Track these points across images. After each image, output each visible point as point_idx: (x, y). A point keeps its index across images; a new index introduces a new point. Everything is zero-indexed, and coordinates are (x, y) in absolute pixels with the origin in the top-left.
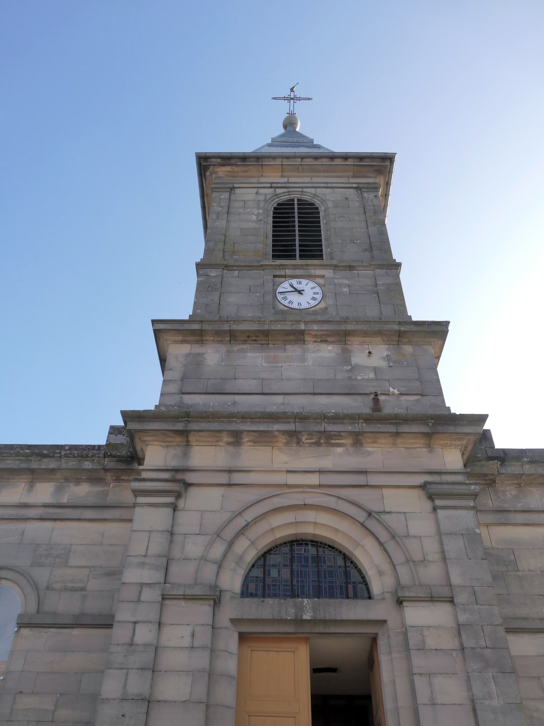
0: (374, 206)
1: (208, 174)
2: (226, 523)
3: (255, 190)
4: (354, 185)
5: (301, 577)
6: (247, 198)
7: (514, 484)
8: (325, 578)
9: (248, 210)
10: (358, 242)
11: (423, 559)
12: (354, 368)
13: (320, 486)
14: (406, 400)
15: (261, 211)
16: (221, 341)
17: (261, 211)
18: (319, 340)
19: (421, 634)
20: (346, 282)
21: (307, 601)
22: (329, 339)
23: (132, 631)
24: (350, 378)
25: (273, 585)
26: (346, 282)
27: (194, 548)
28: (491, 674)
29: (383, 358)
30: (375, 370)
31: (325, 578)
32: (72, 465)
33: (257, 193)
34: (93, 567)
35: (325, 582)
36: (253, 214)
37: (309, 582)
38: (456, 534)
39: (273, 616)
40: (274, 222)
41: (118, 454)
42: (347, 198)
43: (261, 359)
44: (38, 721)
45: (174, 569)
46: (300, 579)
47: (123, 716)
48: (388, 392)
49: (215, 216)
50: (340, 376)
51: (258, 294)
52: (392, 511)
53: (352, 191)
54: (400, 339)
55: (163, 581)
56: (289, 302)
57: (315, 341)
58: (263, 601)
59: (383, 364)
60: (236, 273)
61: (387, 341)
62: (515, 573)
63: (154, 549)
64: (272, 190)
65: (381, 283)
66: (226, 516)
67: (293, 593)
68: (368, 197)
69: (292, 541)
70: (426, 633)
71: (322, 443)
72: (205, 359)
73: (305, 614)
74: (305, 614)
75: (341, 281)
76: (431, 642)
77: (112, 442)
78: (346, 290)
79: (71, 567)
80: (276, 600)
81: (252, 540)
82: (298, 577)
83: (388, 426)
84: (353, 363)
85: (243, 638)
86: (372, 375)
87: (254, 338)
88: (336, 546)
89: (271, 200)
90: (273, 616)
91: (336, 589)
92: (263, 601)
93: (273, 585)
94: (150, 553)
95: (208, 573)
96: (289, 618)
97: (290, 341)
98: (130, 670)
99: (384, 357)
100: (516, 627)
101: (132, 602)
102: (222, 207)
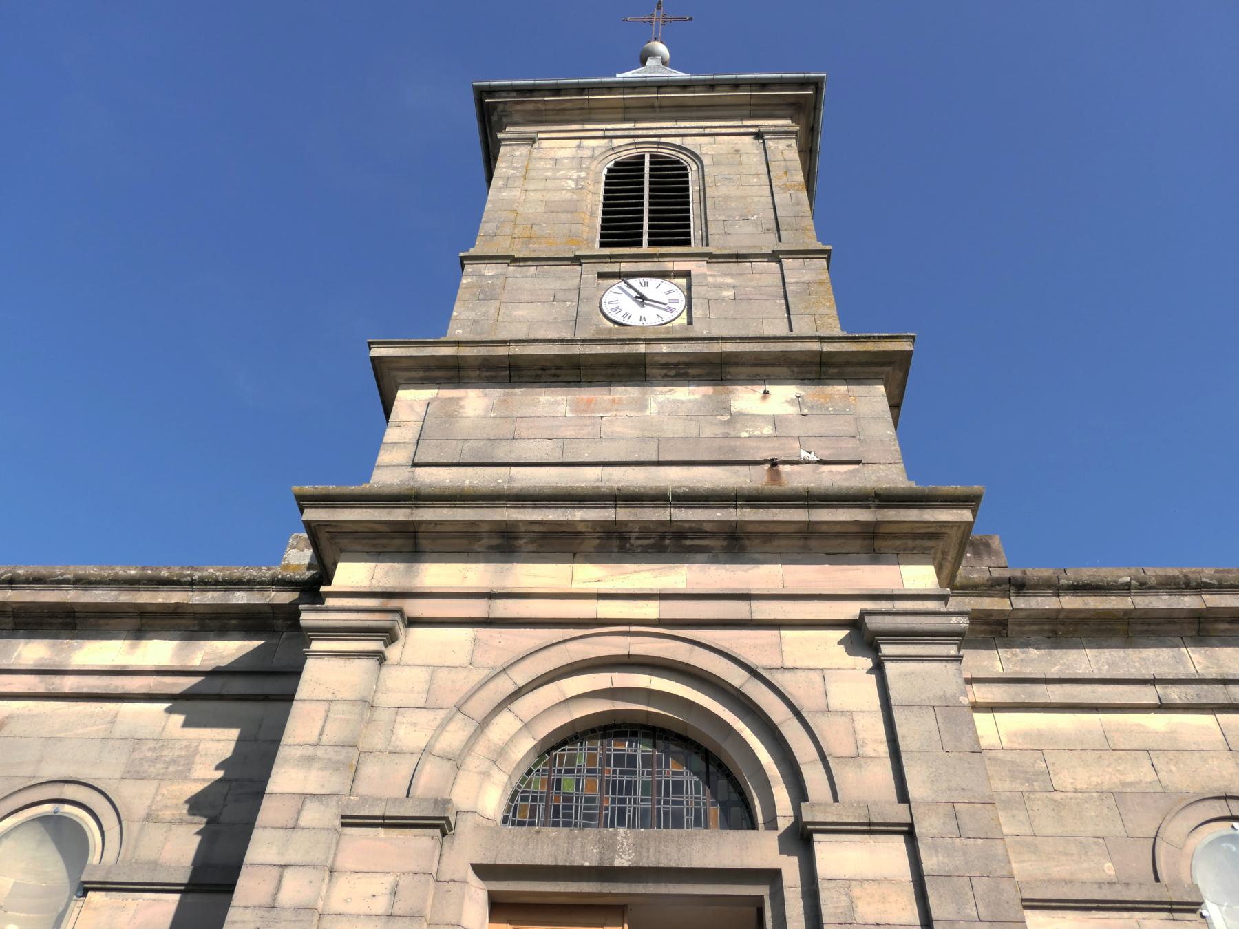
4: (751, 130)
5: (621, 793)
6: (561, 153)
7: (1042, 631)
8: (667, 794)
11: (854, 753)
12: (736, 418)
13: (660, 623)
15: (583, 174)
16: (493, 377)
17: (583, 174)
18: (673, 372)
20: (729, 281)
22: (692, 371)
23: (275, 883)
24: (726, 436)
25: (564, 808)
26: (729, 281)
27: (412, 733)
29: (791, 402)
30: (775, 420)
31: (667, 794)
33: (579, 146)
34: (236, 780)
35: (666, 802)
38: (920, 707)
42: (737, 151)
45: (370, 770)
50: (708, 432)
52: (798, 665)
53: (748, 139)
55: (347, 790)
56: (624, 316)
57: (666, 376)
58: (538, 832)
62: (1048, 794)
63: (334, 732)
66: (477, 676)
70: (856, 891)
71: (667, 547)
72: (462, 407)
75: (720, 280)
77: (292, 562)
78: (729, 294)
79: (195, 780)
81: (526, 721)
82: (613, 793)
84: (733, 409)
86: (768, 430)
87: (553, 371)
88: (691, 736)
92: (538, 832)
93: (564, 808)
94: (325, 739)
95: (430, 778)
96: (587, 864)
97: (620, 375)
100: (1049, 896)
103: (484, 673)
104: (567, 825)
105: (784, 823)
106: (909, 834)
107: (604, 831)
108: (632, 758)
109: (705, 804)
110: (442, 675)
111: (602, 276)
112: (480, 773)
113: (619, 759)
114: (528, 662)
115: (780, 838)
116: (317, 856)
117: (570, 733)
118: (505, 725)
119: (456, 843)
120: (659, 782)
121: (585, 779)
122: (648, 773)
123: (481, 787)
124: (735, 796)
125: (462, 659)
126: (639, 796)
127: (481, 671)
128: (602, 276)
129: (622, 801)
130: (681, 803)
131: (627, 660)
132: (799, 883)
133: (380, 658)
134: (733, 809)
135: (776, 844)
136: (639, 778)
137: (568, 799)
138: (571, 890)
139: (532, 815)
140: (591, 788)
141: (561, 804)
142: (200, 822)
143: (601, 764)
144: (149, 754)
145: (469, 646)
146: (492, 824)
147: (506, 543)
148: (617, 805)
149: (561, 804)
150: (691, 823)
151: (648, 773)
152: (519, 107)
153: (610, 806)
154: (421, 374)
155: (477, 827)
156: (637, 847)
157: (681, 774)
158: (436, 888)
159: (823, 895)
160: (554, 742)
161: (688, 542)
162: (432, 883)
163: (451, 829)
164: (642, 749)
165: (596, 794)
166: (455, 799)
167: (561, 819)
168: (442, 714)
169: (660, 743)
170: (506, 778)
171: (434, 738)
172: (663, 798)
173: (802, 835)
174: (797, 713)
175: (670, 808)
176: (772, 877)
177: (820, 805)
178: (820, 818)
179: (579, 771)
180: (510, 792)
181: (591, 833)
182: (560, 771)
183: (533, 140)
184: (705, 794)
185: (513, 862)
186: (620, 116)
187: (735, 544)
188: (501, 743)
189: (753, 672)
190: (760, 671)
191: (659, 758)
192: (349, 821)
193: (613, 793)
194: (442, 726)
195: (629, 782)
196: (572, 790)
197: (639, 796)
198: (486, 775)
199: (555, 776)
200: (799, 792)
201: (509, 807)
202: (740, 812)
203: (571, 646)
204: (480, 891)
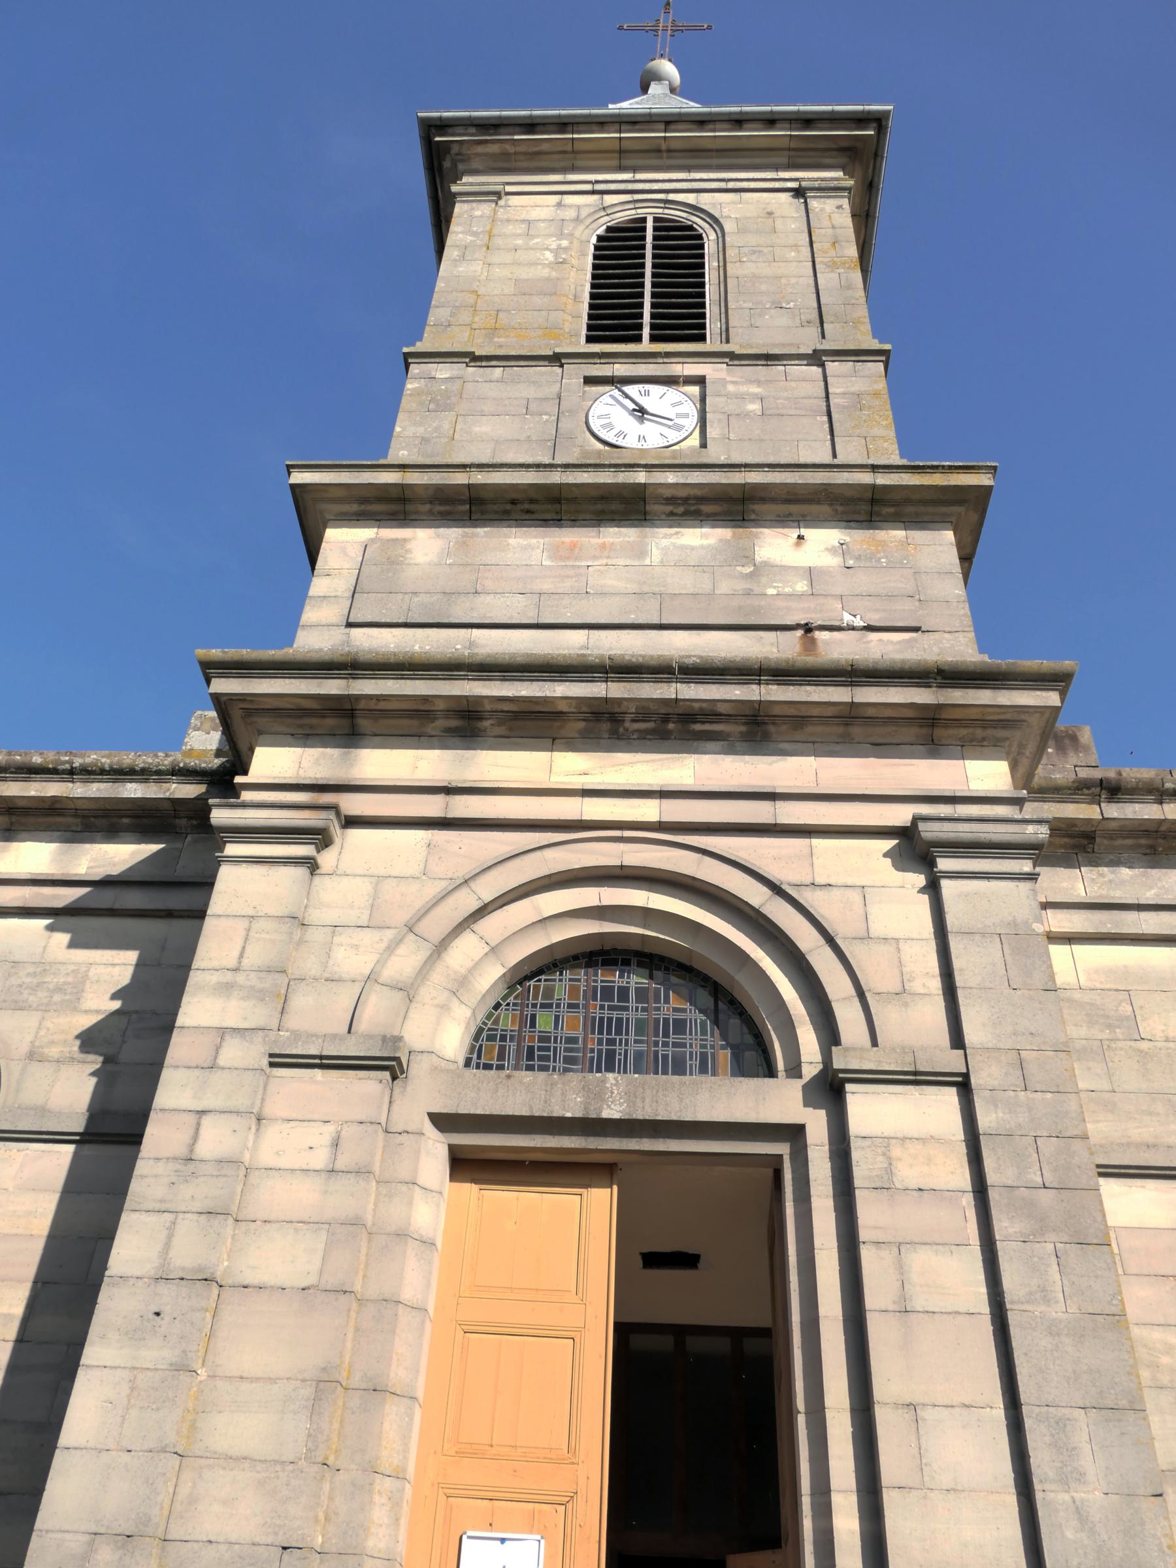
0: (833, 227)
1: (447, 164)
3: (557, 198)
4: (790, 185)
6: (535, 214)
7: (1140, 846)
8: (666, 1035)
9: (536, 240)
10: (792, 305)
11: (899, 989)
12: (760, 570)
13: (661, 827)
14: (881, 640)
15: (565, 243)
17: (565, 243)
18: (681, 509)
19: (884, 1154)
21: (616, 1079)
22: (706, 508)
24: (748, 593)
25: (540, 1049)
27: (354, 957)
28: (1050, 1246)
29: (832, 550)
30: (811, 573)
31: (666, 1035)
32: (98, 790)
34: (136, 1012)
35: (665, 1044)
36: (547, 249)
37: (627, 1044)
38: (983, 934)
39: (531, 1108)
40: (595, 267)
41: (203, 765)
42: (770, 214)
43: (539, 551)
44: (285, 1548)
45: (302, 1001)
46: (605, 1036)
47: (158, 1314)
48: (837, 623)
49: (456, 253)
50: (724, 587)
51: (545, 417)
52: (832, 882)
54: (876, 508)
55: (275, 1025)
57: (672, 514)
58: (509, 1077)
59: (832, 561)
60: (498, 372)
61: (843, 513)
62: (1132, 1043)
63: (256, 956)
64: (596, 197)
65: (838, 391)
66: (433, 889)
68: (822, 210)
69: (591, 952)
70: (896, 1152)
71: (670, 732)
72: (408, 551)
73: (609, 1107)
74: (609, 1107)
75: (744, 389)
76: (908, 1174)
79: (86, 1012)
81: (493, 944)
82: (601, 1032)
83: (831, 689)
84: (758, 559)
85: (463, 1165)
86: (802, 586)
87: (526, 506)
89: (590, 220)
90: (531, 1108)
91: (691, 1059)
92: (509, 1077)
93: (540, 1049)
94: (246, 962)
96: (569, 1115)
97: (613, 512)
98: (181, 1216)
99: (834, 547)
101: (197, 1067)
102: (475, 234)
106: (964, 1086)
109: (712, 1047)
110: (388, 887)
111: (589, 381)
112: (438, 1006)
113: (607, 993)
115: (805, 1088)
116: (241, 1101)
118: (467, 949)
119: (409, 1088)
120: (657, 1021)
122: (644, 1009)
125: (414, 868)
126: (632, 1037)
127: (437, 882)
128: (589, 381)
130: (684, 1045)
131: (619, 872)
132: (826, 1141)
133: (311, 865)
138: (549, 1145)
140: (573, 1026)
141: (536, 1044)
142: (95, 1062)
144: (28, 980)
146: (452, 1067)
147: (466, 725)
148: (604, 1047)
149: (536, 1044)
150: (696, 1069)
151: (644, 1009)
152: (480, 149)
154: (355, 507)
155: (434, 1069)
156: (630, 1096)
157: (684, 1010)
159: (855, 1155)
160: (527, 970)
161: (698, 727)
162: (381, 1134)
164: (636, 980)
165: (579, 1033)
168: (389, 934)
169: (658, 974)
170: (468, 1013)
171: (381, 963)
172: (661, 1039)
173: (831, 1085)
174: (830, 940)
175: (670, 1051)
176: (795, 1133)
177: (854, 1049)
179: (558, 1006)
181: (575, 1079)
182: (534, 1006)
183: (498, 195)
184: (712, 1035)
185: (479, 1112)
186: (615, 163)
187: (757, 730)
188: (463, 971)
189: (776, 889)
191: (657, 991)
192: (279, 1061)
193: (601, 1032)
194: (391, 949)
196: (550, 1028)
197: (632, 1037)
198: (444, 1008)
199: (529, 1011)
202: (756, 1057)
203: (549, 853)
204: (438, 1145)
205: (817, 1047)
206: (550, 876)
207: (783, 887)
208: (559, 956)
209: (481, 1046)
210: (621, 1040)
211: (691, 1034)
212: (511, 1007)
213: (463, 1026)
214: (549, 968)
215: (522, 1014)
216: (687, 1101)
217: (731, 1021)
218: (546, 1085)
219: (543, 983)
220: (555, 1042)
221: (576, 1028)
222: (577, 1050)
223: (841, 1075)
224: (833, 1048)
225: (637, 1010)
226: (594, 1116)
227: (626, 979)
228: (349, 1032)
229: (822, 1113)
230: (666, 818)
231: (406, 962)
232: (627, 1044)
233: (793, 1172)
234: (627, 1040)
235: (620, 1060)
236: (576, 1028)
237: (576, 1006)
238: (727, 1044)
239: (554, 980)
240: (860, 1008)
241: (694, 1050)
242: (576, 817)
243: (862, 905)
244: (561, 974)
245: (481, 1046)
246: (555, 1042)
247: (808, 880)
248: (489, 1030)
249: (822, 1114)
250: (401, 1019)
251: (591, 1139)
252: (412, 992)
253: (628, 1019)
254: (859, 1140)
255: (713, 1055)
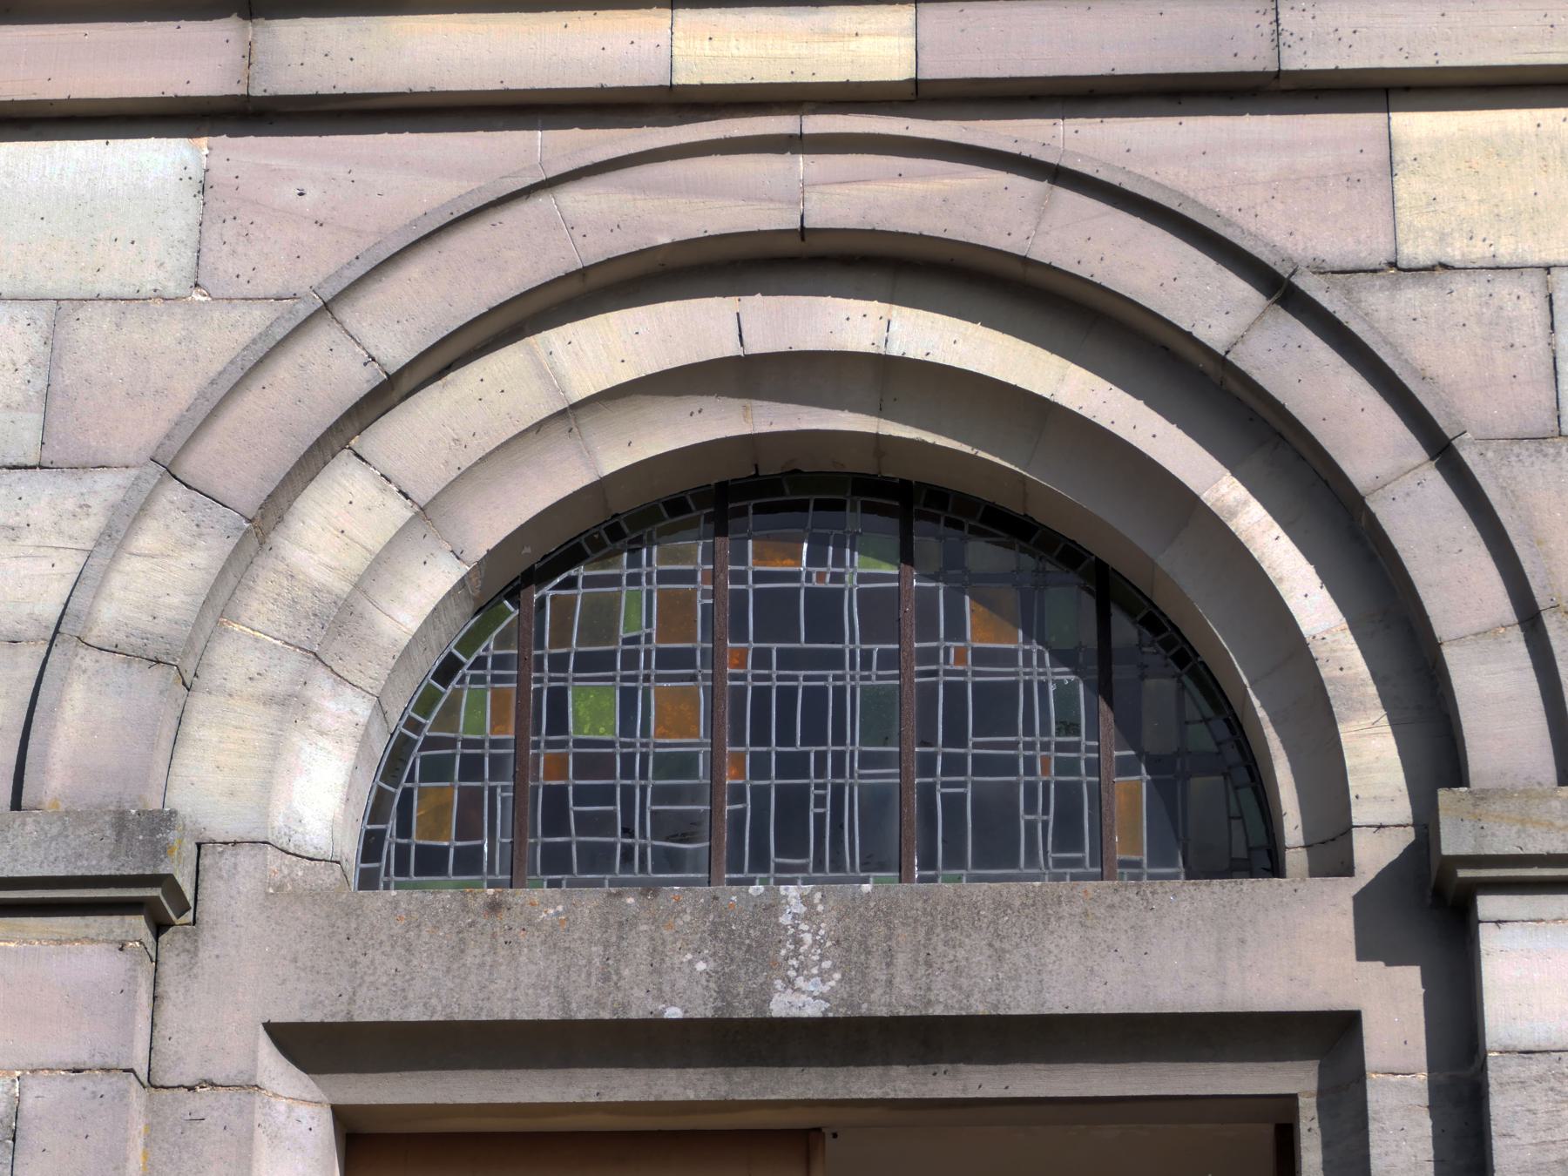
2: (226, 384)
5: (786, 737)
8: (955, 735)
21: (806, 900)
25: (583, 796)
31: (955, 735)
35: (954, 765)
37: (839, 771)
39: (564, 999)
58: (494, 907)
66: (228, 334)
67: (784, 834)
69: (722, 485)
74: (789, 983)
80: (589, 902)
81: (423, 496)
82: (761, 737)
88: (1040, 515)
90: (564, 999)
91: (1031, 808)
92: (494, 907)
93: (583, 796)
96: (674, 1013)
103: (252, 322)
104: (597, 860)
105: (1375, 852)
107: (732, 895)
108: (825, 608)
109: (1094, 767)
110: (93, 328)
112: (270, 700)
113: (776, 611)
114: (415, 270)
115: (1360, 900)
117: (589, 519)
118: (341, 521)
119: (205, 954)
120: (928, 693)
121: (656, 690)
122: (888, 660)
123: (276, 751)
124: (1202, 739)
125: (156, 263)
126: (855, 747)
127: (237, 313)
129: (792, 765)
130: (1009, 766)
131: (795, 246)
132: (1420, 1057)
134: (1198, 784)
135: (1345, 926)
136: (855, 678)
137: (593, 762)
138: (621, 1096)
139: (468, 828)
140: (678, 720)
141: (571, 782)
143: (710, 631)
145: (182, 216)
146: (328, 877)
148: (774, 781)
149: (571, 782)
150: (1046, 841)
151: (888, 660)
153: (749, 783)
155: (276, 893)
156: (851, 950)
157: (1008, 658)
158: (151, 1110)
159: (1500, 1105)
160: (530, 555)
162: (137, 1097)
163: (182, 908)
164: (863, 569)
165: (697, 743)
166: (182, 799)
167: (574, 839)
168: (106, 487)
169: (928, 542)
170: (362, 709)
172: (940, 749)
173: (1438, 893)
174: (1442, 450)
175: (968, 785)
176: (1333, 1036)
177: (1504, 793)
178: (1504, 842)
179: (630, 660)
180: (380, 746)
181: (685, 903)
182: (559, 663)
184: (1093, 733)
185: (414, 1015)
188: (342, 587)
189: (1279, 288)
190: (1308, 284)
191: (926, 602)
193: (761, 737)
194: (114, 537)
195: (815, 697)
196: (609, 730)
197: (855, 747)
198: (290, 705)
199: (543, 682)
200: (1437, 751)
201: (377, 811)
202: (1225, 826)
203: (577, 200)
204: (303, 1111)
205: (1399, 778)
206: (583, 272)
207: (1299, 281)
208: (622, 504)
209: (407, 794)
210: (821, 757)
211: (1029, 730)
212: (489, 672)
213: (350, 749)
214: (597, 545)
215: (522, 691)
216: (1017, 958)
217: (1150, 683)
218: (605, 926)
219: (580, 591)
220: (628, 772)
221: (687, 729)
222: (693, 794)
223: (1463, 873)
224: (1444, 795)
225: (866, 664)
226: (749, 1013)
227: (830, 568)
228: (16, 804)
229: (1410, 977)
230: (935, 70)
231: (162, 573)
232: (839, 771)
233: (1326, 1145)
234: (839, 758)
235: (820, 818)
236: (687, 729)
237: (685, 659)
238: (1140, 753)
239: (615, 580)
240: (1527, 662)
241: (1040, 778)
242: (654, 77)
243: (1541, 331)
244: (634, 562)
245: (407, 794)
246: (628, 772)
247: (1377, 253)
248: (430, 743)
249: (1408, 981)
250: (165, 745)
251: (743, 1073)
252: (189, 666)
253: (839, 692)
254: (1514, 1060)
255: (1097, 793)
